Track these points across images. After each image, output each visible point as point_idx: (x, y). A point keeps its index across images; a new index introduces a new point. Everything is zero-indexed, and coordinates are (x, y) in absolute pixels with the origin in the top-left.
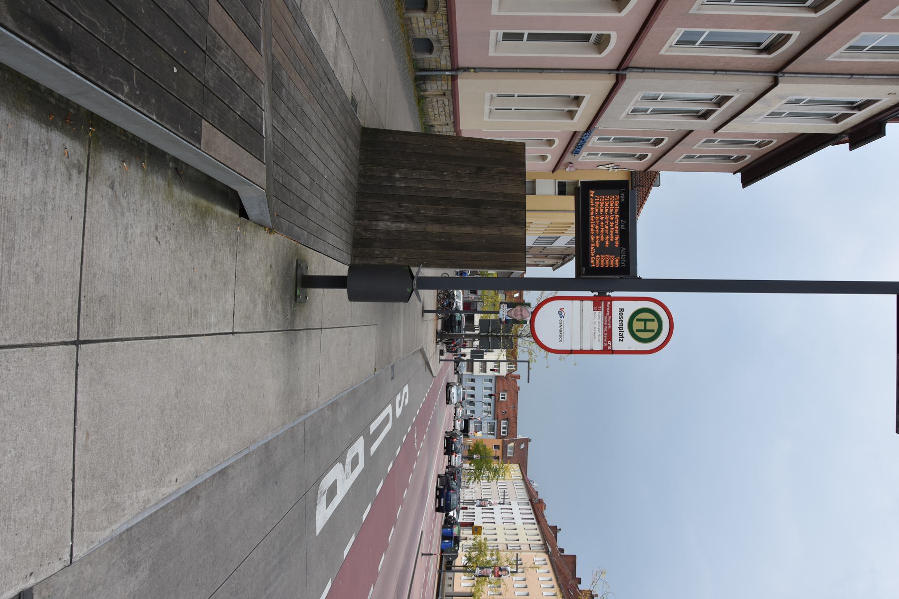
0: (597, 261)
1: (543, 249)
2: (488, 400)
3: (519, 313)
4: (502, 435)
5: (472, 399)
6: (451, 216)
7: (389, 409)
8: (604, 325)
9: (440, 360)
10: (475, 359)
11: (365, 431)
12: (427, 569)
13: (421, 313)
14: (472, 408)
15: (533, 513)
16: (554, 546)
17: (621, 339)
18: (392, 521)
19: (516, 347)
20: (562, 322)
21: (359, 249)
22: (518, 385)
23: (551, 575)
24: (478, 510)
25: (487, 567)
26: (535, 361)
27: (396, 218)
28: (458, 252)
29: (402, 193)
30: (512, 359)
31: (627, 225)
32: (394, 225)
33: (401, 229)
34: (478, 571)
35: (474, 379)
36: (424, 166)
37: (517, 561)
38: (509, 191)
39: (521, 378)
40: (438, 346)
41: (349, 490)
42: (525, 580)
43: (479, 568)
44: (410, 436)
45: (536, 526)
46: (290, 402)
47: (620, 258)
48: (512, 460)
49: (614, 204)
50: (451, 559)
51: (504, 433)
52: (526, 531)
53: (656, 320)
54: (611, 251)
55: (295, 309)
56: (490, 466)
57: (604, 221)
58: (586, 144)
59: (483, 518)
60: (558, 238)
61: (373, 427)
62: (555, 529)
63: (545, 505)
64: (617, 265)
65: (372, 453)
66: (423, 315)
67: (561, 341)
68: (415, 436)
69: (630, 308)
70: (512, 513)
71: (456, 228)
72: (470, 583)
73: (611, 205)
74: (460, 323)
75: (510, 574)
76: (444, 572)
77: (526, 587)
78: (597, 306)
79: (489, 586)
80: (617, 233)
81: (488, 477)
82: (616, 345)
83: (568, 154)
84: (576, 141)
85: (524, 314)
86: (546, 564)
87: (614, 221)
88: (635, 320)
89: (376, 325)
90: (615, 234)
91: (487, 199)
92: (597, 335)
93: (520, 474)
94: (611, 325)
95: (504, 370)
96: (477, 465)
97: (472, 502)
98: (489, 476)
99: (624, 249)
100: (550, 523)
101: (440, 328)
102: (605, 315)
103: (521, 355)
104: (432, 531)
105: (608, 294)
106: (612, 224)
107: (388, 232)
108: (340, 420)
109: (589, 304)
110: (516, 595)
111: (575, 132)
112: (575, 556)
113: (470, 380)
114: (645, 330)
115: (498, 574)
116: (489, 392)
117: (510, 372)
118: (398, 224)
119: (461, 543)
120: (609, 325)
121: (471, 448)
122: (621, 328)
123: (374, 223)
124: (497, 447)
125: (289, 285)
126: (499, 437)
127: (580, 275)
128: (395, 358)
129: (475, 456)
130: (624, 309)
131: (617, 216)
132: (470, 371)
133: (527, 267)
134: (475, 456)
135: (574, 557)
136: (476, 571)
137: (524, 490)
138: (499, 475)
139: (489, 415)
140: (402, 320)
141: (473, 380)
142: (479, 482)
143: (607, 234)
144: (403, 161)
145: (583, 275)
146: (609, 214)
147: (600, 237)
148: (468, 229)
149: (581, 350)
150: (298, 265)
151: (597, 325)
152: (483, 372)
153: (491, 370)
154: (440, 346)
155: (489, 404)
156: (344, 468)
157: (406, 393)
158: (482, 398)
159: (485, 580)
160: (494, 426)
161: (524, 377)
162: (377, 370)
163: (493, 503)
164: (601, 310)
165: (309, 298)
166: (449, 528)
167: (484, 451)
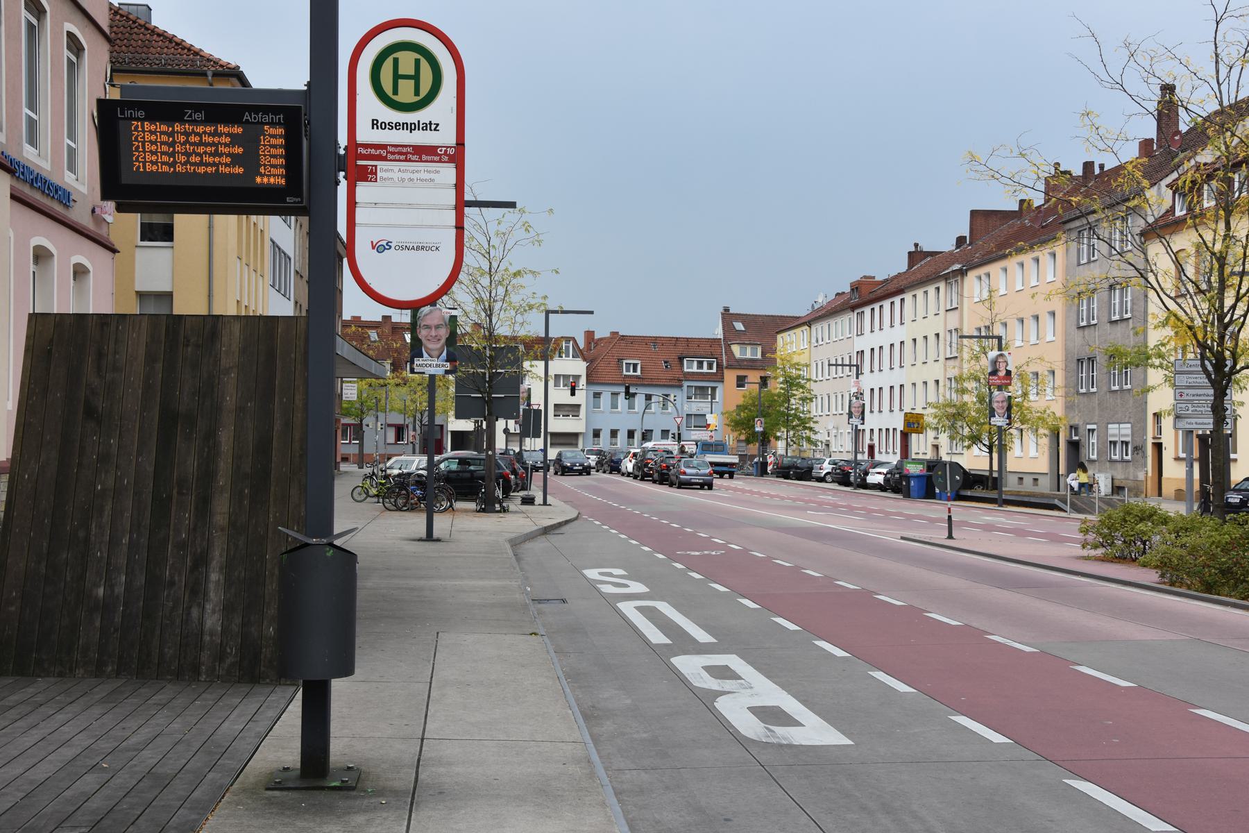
0: (272, 176)
1: (301, 277)
2: (639, 401)
3: (433, 333)
4: (714, 370)
5: (638, 436)
6: (195, 473)
7: (627, 608)
8: (406, 160)
11: (661, 654)
12: (989, 528)
15: (880, 304)
16: (950, 258)
17: (433, 127)
18: (865, 599)
19: (514, 338)
20: (400, 245)
21: (262, 669)
22: (608, 335)
23: (1012, 263)
24: (873, 421)
25: (990, 401)
26: (545, 297)
27: (197, 591)
28: (274, 458)
29: (140, 580)
30: (545, 348)
31: (197, 107)
32: (212, 595)
33: (222, 581)
34: (999, 421)
35: (594, 430)
36: (81, 534)
37: (980, 337)
38: (142, 351)
39: (591, 330)
40: (512, 507)
41: (776, 683)
42: (1022, 321)
43: (992, 419)
44: (691, 564)
45: (908, 297)
46: (559, 793)
47: (267, 124)
48: (769, 349)
49: (151, 132)
50: (958, 478)
51: (710, 367)
52: (919, 318)
53: (395, 55)
54: (250, 143)
55: (369, 790)
56: (779, 395)
57: (188, 154)
58: (44, 175)
59: (891, 411)
60: (273, 242)
61: (656, 636)
62: (916, 256)
63: (865, 277)
64: (281, 131)
65: (712, 640)
66: (438, 540)
67: (437, 248)
68: (697, 553)
69: (369, 106)
70: (881, 348)
71: (222, 465)
72: (1029, 437)
73: (153, 138)
74: (463, 461)
75: (1005, 353)
76: (1001, 493)
77: (1037, 318)
78: (366, 175)
79: (1032, 397)
80: (213, 128)
81: (804, 400)
82: (445, 137)
83: (69, 216)
84: (37, 197)
85: (436, 322)
86: (988, 275)
87: (187, 134)
88: (395, 98)
89: (438, 633)
90: (215, 134)
91: (158, 399)
92: (427, 176)
93: (798, 331)
94: (406, 146)
95: (577, 367)
96: (778, 424)
97: (857, 433)
98: (801, 399)
99: (247, 116)
100: (903, 267)
101: (472, 505)
102: (385, 159)
103: (533, 327)
104: (909, 517)
105: (342, 152)
106: (193, 139)
107: (228, 609)
108: (629, 701)
109: (364, 191)
110: (1054, 339)
111: (13, 197)
114: (416, 78)
115: (1004, 378)
116: (622, 400)
117: (578, 353)
118: (212, 586)
119: (946, 458)
120: (405, 150)
121: (743, 437)
122: (412, 127)
123: (207, 638)
124: (741, 382)
125: (317, 802)
126: (719, 377)
127: (304, 208)
128: (517, 596)
129: (757, 429)
130: (373, 120)
131: (178, 127)
133: (174, 313)
134: (758, 429)
135: (974, 214)
136: (999, 424)
137: (832, 322)
138: (799, 377)
139: (672, 398)
140: (440, 582)
141: (597, 434)
142: (815, 419)
143: (217, 150)
144: (68, 579)
145: (302, 202)
146: (172, 144)
147: (222, 164)
148: (226, 437)
149: (456, 208)
150: (278, 786)
151: (406, 176)
152: (579, 411)
153: (573, 394)
154: (514, 504)
155: (648, 397)
156: (729, 693)
157: (601, 574)
158: (636, 413)
159: (1019, 405)
160: (696, 387)
161: (585, 323)
162: (535, 631)
163: (854, 390)
164: (376, 166)
165: (352, 762)
166: (908, 483)
167: (750, 410)
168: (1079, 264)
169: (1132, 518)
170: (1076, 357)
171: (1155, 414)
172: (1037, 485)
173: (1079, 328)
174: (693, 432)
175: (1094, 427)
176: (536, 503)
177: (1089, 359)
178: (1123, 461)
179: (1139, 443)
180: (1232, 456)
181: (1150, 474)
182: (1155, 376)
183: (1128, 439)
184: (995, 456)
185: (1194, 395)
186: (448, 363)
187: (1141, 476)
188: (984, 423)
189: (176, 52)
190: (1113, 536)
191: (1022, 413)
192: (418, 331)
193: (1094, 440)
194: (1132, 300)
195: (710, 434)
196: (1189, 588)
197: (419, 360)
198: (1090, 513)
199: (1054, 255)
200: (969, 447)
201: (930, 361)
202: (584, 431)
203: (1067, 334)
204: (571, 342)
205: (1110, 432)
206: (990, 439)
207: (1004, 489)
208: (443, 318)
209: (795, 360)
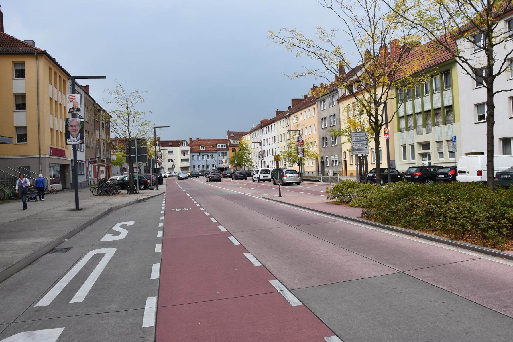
2: (205, 157)
3: (74, 128)
4: (226, 147)
5: (205, 167)
9: (157, 189)
10: (155, 167)
13: (79, 211)
14: (211, 166)
16: (287, 112)
22: (196, 139)
23: (303, 111)
34: (300, 156)
35: (193, 166)
39: (191, 138)
45: (276, 123)
51: (225, 147)
52: (279, 129)
59: (268, 156)
62: (278, 113)
68: (180, 210)
72: (310, 160)
75: (301, 135)
77: (310, 127)
85: (75, 124)
86: (297, 115)
93: (247, 135)
98: (247, 154)
100: (274, 116)
101: (126, 191)
110: (315, 132)
112: (292, 99)
113: (204, 168)
115: (301, 143)
117: (187, 144)
126: (227, 149)
129: (235, 163)
132: (188, 169)
135: (293, 100)
137: (256, 132)
138: (247, 147)
141: (194, 167)
152: (188, 161)
153: (184, 156)
155: (208, 156)
168: (321, 111)
169: (346, 187)
170: (322, 137)
171: (344, 152)
172: (313, 174)
173: (322, 129)
174: (221, 165)
175: (328, 157)
176: (155, 189)
177: (325, 137)
178: (336, 166)
179: (340, 161)
180: (381, 162)
181: (343, 169)
182: (344, 139)
183: (337, 160)
184: (300, 166)
185: (357, 144)
186: (81, 140)
187: (341, 170)
188: (296, 157)
189: (14, 42)
190: (338, 194)
191: (307, 153)
192: (68, 128)
193: (328, 161)
194: (336, 120)
195: (224, 165)
196: (375, 220)
197: (69, 139)
198: (328, 182)
199: (314, 108)
200: (293, 164)
201: (283, 141)
202: (190, 166)
203: (319, 131)
204: (185, 142)
205: (332, 158)
206: (299, 161)
207: (303, 176)
208: (78, 122)
209: (245, 143)
